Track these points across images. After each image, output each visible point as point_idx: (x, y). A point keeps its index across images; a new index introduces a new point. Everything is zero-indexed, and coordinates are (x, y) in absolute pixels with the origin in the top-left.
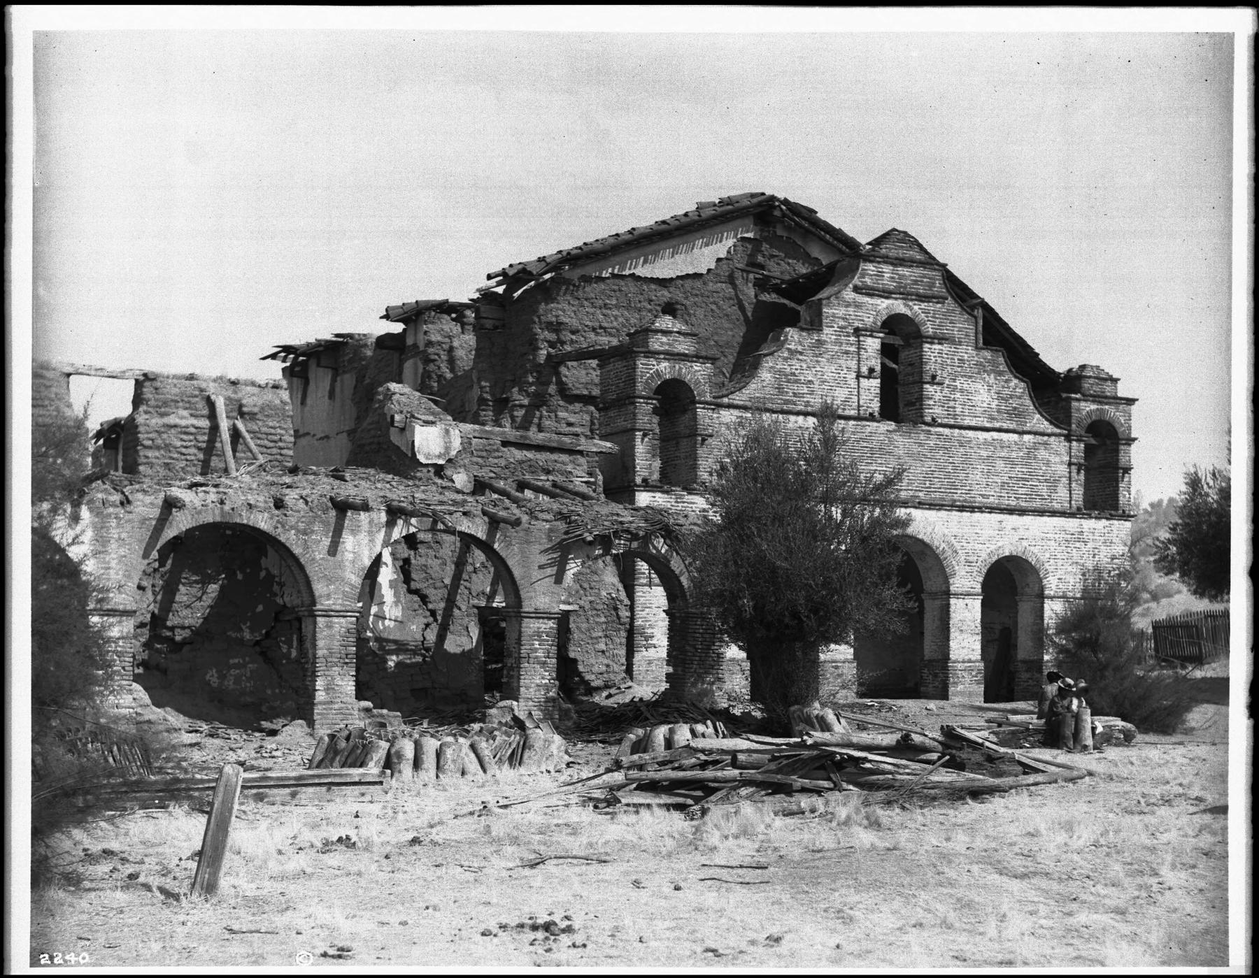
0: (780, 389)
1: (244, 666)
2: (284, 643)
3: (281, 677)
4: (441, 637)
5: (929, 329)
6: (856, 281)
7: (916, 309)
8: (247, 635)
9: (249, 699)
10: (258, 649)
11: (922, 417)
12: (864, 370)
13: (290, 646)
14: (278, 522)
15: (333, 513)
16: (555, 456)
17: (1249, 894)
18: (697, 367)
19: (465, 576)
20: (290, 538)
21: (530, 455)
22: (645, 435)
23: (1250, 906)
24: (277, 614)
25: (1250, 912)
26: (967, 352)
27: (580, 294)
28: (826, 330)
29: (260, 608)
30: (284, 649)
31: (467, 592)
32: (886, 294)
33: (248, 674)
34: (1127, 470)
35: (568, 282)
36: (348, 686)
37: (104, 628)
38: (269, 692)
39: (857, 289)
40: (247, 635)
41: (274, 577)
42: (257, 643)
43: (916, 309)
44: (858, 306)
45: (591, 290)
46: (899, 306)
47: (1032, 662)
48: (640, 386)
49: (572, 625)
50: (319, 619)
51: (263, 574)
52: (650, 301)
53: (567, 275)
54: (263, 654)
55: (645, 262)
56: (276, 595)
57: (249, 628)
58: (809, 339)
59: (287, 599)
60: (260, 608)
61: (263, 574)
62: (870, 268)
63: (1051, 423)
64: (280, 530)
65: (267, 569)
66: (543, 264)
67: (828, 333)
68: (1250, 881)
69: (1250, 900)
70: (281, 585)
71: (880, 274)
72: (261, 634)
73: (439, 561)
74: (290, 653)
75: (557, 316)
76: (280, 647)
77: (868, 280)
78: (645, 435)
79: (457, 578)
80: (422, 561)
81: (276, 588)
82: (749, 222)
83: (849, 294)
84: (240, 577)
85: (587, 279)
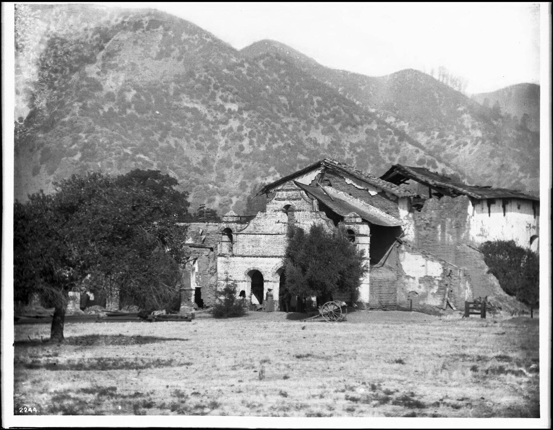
0: (255, 228)
5: (297, 208)
6: (276, 197)
7: (293, 203)
16: (202, 249)
17: (550, 412)
18: (233, 224)
21: (196, 249)
23: (550, 385)
25: (551, 329)
26: (308, 213)
28: (268, 211)
32: (284, 200)
34: (131, 171)
37: (424, 304)
39: (276, 199)
43: (293, 203)
44: (276, 204)
46: (288, 202)
58: (263, 214)
62: (280, 193)
67: (268, 212)
68: (551, 299)
69: (550, 326)
71: (283, 195)
77: (279, 197)
83: (274, 201)
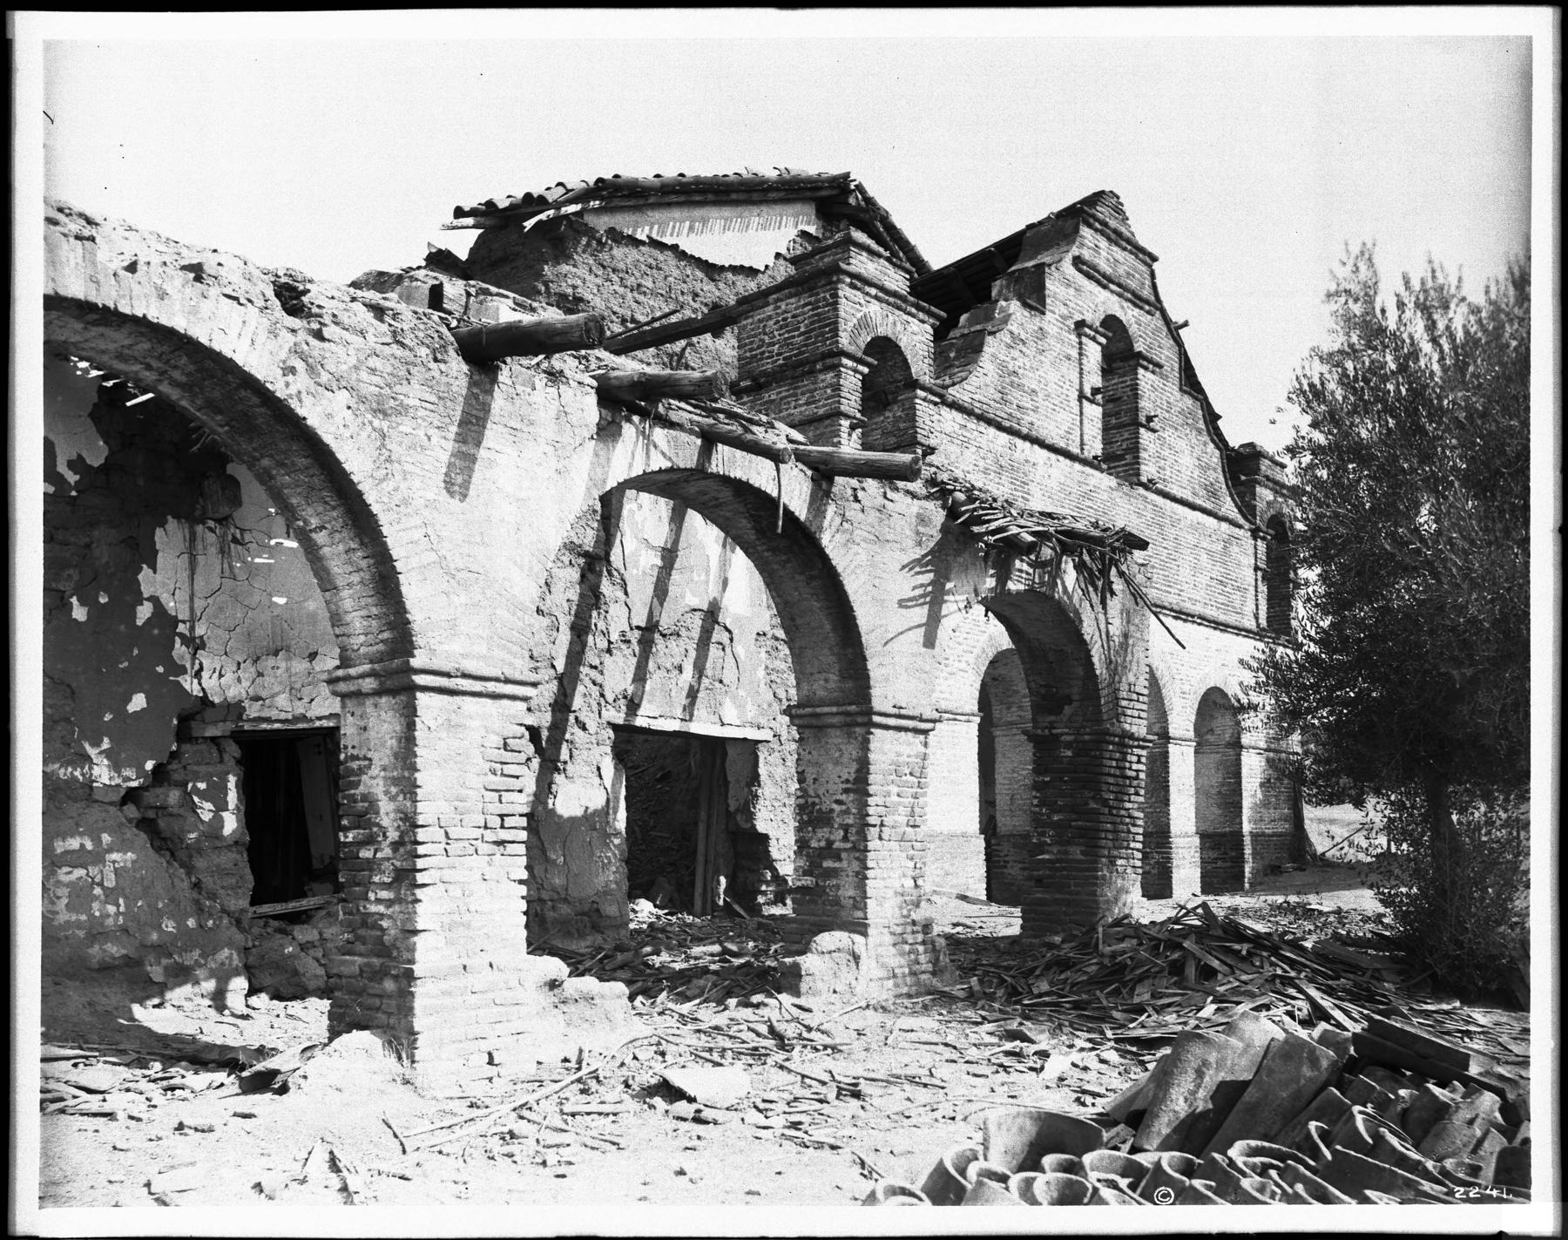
1: (98, 857)
2: (204, 795)
3: (197, 886)
4: (545, 787)
6: (1075, 251)
8: (102, 773)
9: (114, 950)
10: (131, 811)
11: (1138, 475)
12: (1088, 391)
13: (221, 806)
14: (296, 351)
15: (457, 367)
19: (591, 657)
20: (326, 415)
22: (853, 428)
24: (185, 719)
27: (604, 256)
29: (138, 702)
30: (206, 811)
31: (595, 691)
33: (110, 882)
35: (590, 232)
36: (508, 909)
38: (169, 926)
40: (102, 773)
41: (175, 621)
42: (131, 796)
45: (621, 255)
47: (1223, 835)
48: (844, 341)
49: (762, 770)
50: (422, 699)
51: (144, 612)
52: (696, 295)
53: (591, 220)
54: (147, 825)
55: (691, 228)
56: (183, 670)
57: (107, 754)
59: (210, 682)
60: (138, 702)
61: (144, 612)
63: (1241, 511)
64: (301, 381)
65: (155, 600)
66: (561, 190)
70: (196, 645)
72: (141, 772)
73: (546, 621)
74: (218, 822)
75: (574, 287)
76: (193, 808)
78: (853, 428)
79: (576, 656)
80: (1029, 419)
81: (180, 650)
82: (810, 210)
84: (79, 613)
85: (616, 236)
